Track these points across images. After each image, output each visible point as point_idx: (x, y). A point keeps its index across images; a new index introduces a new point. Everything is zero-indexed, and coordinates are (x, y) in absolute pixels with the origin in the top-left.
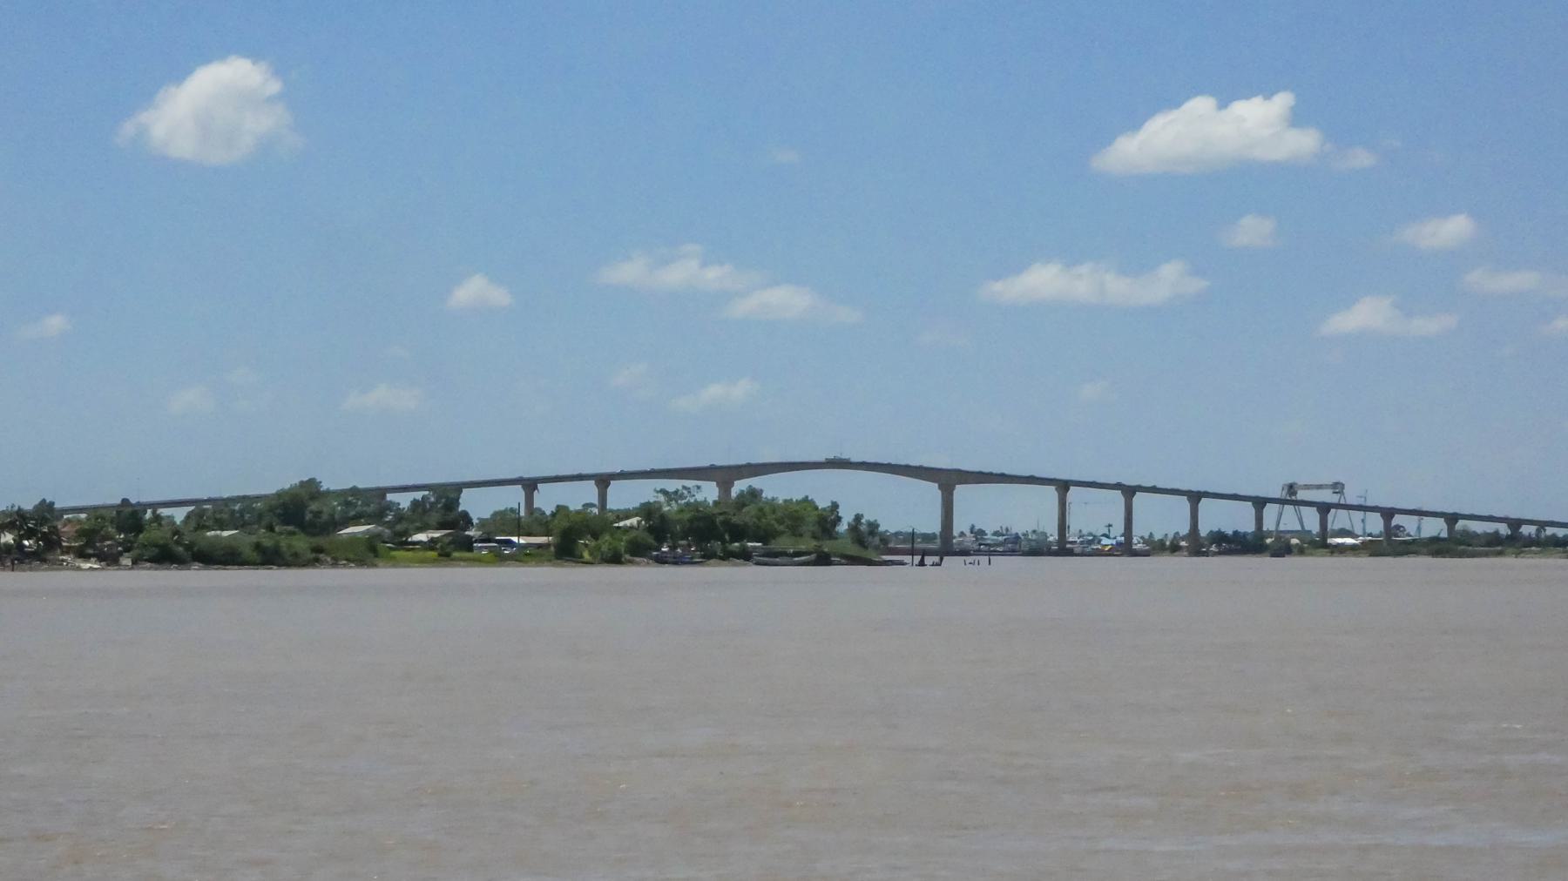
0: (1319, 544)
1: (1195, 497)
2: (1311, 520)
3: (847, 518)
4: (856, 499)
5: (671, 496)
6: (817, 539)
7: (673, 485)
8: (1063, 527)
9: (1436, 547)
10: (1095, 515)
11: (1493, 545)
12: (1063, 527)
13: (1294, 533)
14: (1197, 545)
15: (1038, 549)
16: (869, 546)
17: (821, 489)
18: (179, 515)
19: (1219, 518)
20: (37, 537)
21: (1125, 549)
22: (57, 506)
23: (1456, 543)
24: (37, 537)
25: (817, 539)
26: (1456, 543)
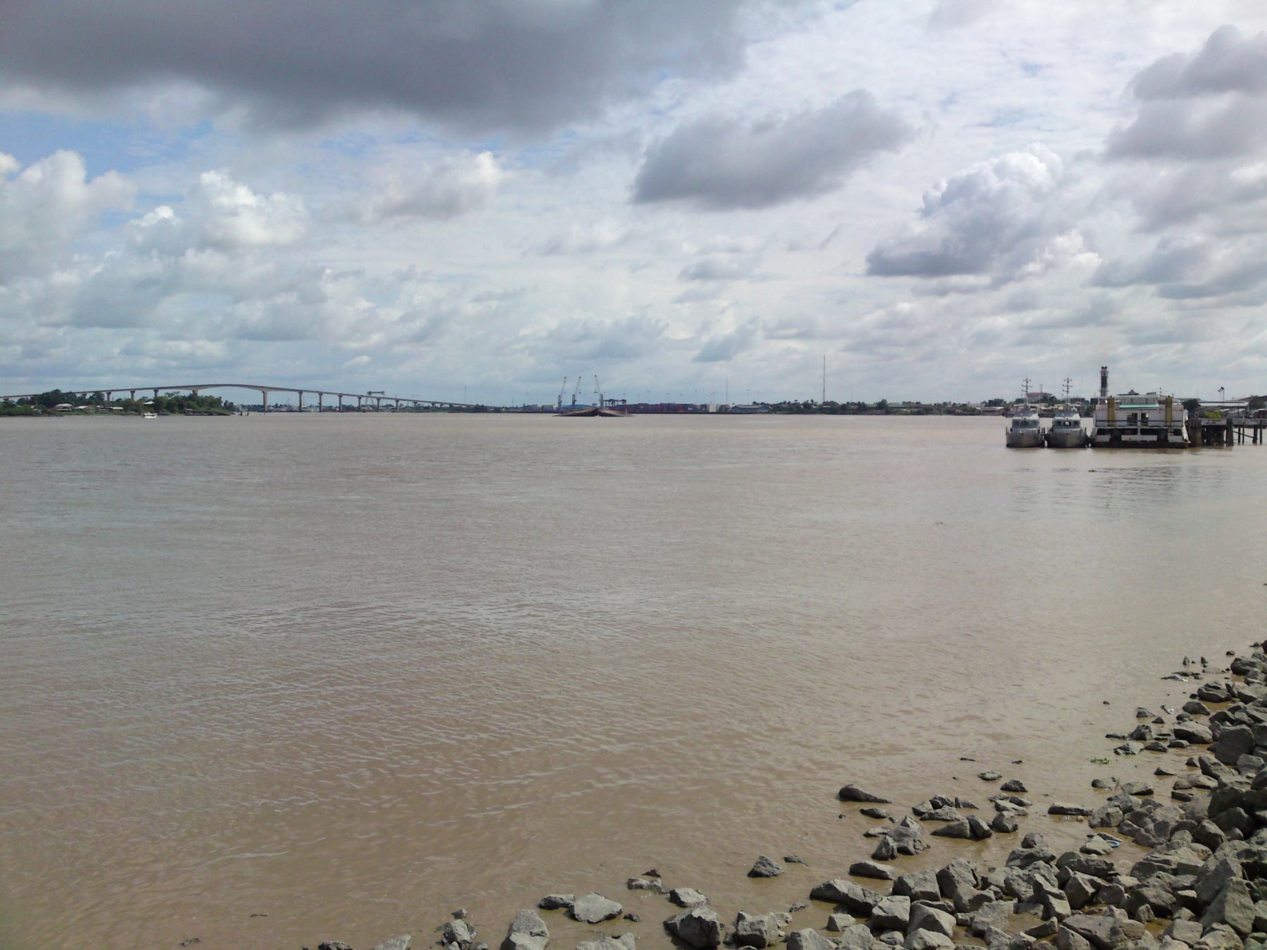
0: (376, 409)
1: (340, 396)
2: (376, 403)
3: (224, 400)
4: (227, 395)
5: (170, 395)
6: (212, 407)
7: (170, 391)
8: (560, 402)
9: (394, 410)
10: (310, 400)
11: (427, 409)
12: (560, 402)
13: (1087, 408)
14: (322, 409)
15: (290, 410)
16: (230, 408)
17: (214, 393)
18: (16, 400)
19: (331, 401)
20: (7, 409)
21: (300, 410)
22: (922, 205)
23: (418, 408)
24: (7, 409)
25: (212, 407)
26: (418, 408)
